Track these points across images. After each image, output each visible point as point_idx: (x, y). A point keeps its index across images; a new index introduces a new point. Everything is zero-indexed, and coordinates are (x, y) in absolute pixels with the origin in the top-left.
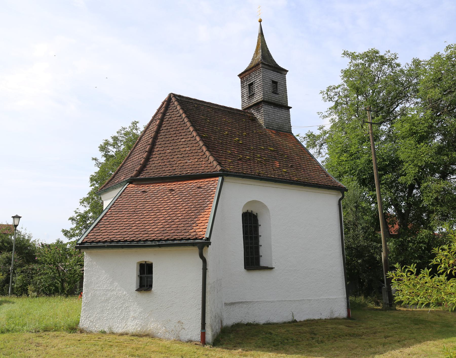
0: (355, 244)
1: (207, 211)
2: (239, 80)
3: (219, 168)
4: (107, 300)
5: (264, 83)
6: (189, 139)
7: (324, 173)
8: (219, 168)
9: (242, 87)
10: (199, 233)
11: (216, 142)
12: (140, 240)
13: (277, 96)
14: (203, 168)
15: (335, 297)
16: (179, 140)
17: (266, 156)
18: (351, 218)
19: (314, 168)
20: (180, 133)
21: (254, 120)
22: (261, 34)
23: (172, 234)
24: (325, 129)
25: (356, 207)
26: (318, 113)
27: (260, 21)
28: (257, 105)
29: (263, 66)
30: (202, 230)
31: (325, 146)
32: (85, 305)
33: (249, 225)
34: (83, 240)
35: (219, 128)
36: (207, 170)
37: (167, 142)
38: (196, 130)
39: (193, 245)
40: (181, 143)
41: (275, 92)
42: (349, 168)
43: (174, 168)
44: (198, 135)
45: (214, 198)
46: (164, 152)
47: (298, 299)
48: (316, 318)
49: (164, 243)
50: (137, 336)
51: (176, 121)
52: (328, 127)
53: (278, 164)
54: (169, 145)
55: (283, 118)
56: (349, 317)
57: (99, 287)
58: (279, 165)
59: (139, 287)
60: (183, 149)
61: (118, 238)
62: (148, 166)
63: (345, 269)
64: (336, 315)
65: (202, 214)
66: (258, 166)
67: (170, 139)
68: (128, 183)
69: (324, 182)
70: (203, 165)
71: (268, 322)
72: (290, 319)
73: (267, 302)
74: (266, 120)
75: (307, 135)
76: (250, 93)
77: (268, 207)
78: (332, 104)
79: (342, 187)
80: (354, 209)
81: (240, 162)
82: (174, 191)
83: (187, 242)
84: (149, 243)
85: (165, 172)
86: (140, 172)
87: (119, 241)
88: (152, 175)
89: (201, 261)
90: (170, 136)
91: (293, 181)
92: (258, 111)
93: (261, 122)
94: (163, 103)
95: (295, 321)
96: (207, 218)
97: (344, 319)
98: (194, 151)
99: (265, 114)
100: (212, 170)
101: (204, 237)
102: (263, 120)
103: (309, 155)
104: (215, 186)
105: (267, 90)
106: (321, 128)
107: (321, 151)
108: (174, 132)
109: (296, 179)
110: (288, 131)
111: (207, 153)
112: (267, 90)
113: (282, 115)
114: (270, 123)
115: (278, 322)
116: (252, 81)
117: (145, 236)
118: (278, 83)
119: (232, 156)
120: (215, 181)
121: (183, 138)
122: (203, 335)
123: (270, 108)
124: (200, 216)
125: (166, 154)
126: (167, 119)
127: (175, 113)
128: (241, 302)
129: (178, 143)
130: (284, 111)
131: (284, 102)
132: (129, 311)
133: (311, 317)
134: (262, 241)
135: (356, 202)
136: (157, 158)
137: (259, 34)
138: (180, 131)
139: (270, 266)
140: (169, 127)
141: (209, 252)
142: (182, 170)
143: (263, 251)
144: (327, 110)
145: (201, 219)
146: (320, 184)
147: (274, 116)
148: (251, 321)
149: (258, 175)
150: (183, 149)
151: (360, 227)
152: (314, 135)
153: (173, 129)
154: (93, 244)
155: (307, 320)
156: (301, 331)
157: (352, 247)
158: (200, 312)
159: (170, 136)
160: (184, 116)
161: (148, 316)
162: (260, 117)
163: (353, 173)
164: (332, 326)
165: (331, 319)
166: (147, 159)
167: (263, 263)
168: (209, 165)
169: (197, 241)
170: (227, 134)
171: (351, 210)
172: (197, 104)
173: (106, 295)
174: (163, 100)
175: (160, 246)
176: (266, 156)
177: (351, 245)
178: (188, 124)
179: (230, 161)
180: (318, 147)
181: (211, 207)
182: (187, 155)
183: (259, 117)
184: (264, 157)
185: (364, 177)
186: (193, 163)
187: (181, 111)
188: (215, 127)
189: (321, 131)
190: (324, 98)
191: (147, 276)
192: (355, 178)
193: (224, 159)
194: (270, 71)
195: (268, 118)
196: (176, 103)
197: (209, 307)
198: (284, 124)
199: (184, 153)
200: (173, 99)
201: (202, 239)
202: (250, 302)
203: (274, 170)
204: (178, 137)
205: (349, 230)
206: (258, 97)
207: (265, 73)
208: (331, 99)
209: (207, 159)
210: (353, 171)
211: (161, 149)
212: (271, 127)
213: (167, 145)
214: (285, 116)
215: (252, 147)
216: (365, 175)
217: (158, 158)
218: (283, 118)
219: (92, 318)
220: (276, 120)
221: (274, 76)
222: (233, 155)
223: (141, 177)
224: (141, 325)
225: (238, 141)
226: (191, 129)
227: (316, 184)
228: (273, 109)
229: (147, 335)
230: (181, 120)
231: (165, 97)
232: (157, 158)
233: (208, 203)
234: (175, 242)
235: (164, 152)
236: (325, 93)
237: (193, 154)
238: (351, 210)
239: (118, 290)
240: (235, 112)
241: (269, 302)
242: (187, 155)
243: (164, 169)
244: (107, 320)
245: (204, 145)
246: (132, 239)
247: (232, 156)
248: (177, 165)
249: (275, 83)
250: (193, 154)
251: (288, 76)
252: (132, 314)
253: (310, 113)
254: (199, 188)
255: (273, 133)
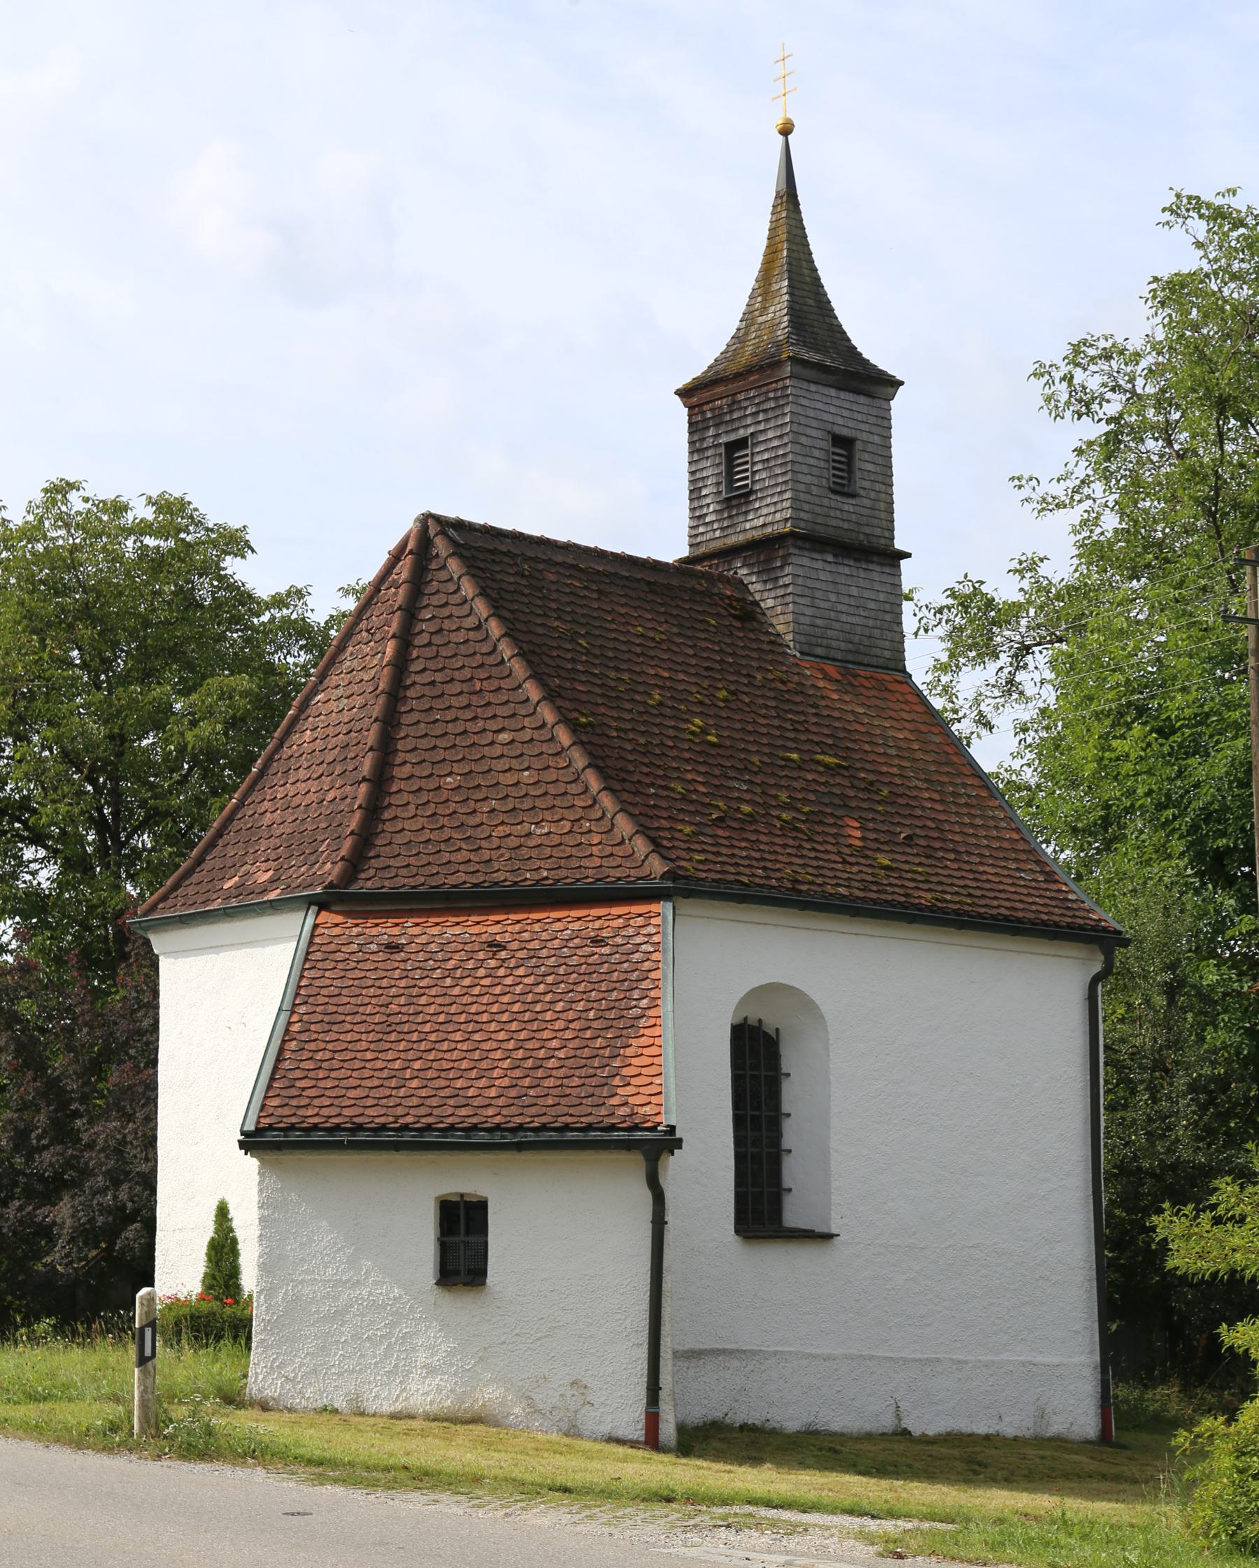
0: (1155, 1154)
1: (647, 1032)
2: (680, 413)
3: (657, 866)
4: (339, 1315)
5: (798, 448)
6: (527, 735)
7: (1038, 862)
8: (657, 866)
9: (697, 449)
10: (642, 1110)
11: (628, 746)
12: (452, 1127)
13: (848, 505)
14: (597, 862)
15: (1056, 1360)
16: (489, 737)
17: (812, 797)
18: (1144, 1037)
19: (996, 844)
20: (489, 704)
21: (749, 614)
22: (788, 197)
23: (552, 1111)
24: (1044, 570)
25: (1171, 991)
26: (1018, 481)
27: (786, 131)
28: (764, 550)
29: (800, 370)
30: (647, 1099)
31: (1039, 659)
32: (265, 1329)
33: (749, 1073)
34: (258, 1122)
35: (625, 677)
36: (613, 873)
37: (439, 742)
38: (551, 696)
39: (627, 1145)
40: (497, 750)
41: (843, 487)
42: (1149, 793)
43: (486, 855)
44: (565, 720)
45: (661, 984)
46: (432, 784)
47: (918, 1356)
48: (982, 1429)
49: (531, 1137)
50: (446, 1420)
51: (463, 649)
52: (1062, 567)
53: (858, 834)
54: (449, 755)
55: (872, 605)
56: (1104, 1437)
57: (307, 1272)
58: (863, 839)
59: (438, 1276)
60: (510, 778)
61: (374, 1115)
62: (379, 842)
63: (1103, 1269)
64: (1057, 1427)
65: (634, 1042)
66: (785, 846)
67: (451, 728)
68: (314, 909)
69: (1035, 907)
70: (595, 850)
71: (813, 1428)
72: (886, 1423)
73: (809, 1356)
74: (803, 620)
75: (953, 594)
76: (730, 488)
77: (824, 1009)
78: (1094, 430)
79: (1105, 929)
80: (1160, 1001)
81: (720, 832)
82: (505, 948)
83: (606, 1136)
84: (482, 1137)
85: (453, 868)
86: (355, 863)
87: (383, 1127)
88: (405, 882)
89: (646, 1196)
90: (450, 715)
91: (919, 907)
92: (768, 573)
93: (781, 629)
94: (396, 557)
95: (906, 1433)
96: (656, 1060)
97: (1088, 1442)
98: (552, 789)
99: (799, 591)
100: (633, 872)
101: (659, 1124)
102: (790, 618)
103: (976, 782)
104: (656, 939)
105: (808, 479)
106: (1027, 566)
107: (1019, 677)
108: (463, 700)
109: (926, 898)
110: (892, 664)
111: (607, 801)
112: (808, 479)
113: (867, 594)
114: (818, 632)
115: (845, 1430)
116: (742, 433)
117: (463, 1112)
118: (859, 445)
119: (692, 808)
120: (648, 916)
121: (502, 730)
122: (652, 1421)
123: (820, 565)
124: (629, 1052)
125: (445, 795)
126: (425, 638)
127: (456, 611)
128: (724, 1352)
129: (487, 751)
130: (876, 572)
131: (878, 532)
132: (414, 1350)
133: (964, 1425)
134: (790, 1137)
135: (1172, 967)
136: (411, 810)
137: (778, 196)
138: (489, 697)
139: (820, 1228)
140: (439, 677)
141: (674, 1168)
142: (517, 865)
143: (793, 1172)
144: (1062, 471)
145: (635, 1061)
146: (1019, 920)
147: (833, 598)
148: (755, 1418)
149: (793, 889)
150: (510, 778)
151: (1181, 1081)
152: (990, 603)
153: (457, 687)
154: (294, 1136)
155: (949, 1434)
156: (934, 1453)
157: (1139, 1169)
158: (643, 1353)
159: (450, 715)
160: (495, 628)
161: (474, 1366)
162: (779, 605)
163: (1167, 822)
164: (1042, 1453)
165: (1040, 1441)
166: (374, 810)
167: (793, 1216)
168: (618, 851)
169: (639, 1135)
170: (661, 704)
171: (1147, 1001)
172: (528, 559)
173: (336, 1299)
174: (393, 543)
175: (520, 1147)
176: (812, 797)
177: (1135, 1158)
178: (518, 668)
179: (688, 830)
180: (1004, 659)
181: (658, 1021)
182: (527, 804)
183: (770, 603)
184: (805, 801)
185: (1222, 842)
186: (556, 840)
187: (481, 608)
188: (613, 674)
189: (1026, 584)
190: (1048, 399)
191: (466, 1239)
192: (1177, 845)
193: (665, 824)
194: (826, 391)
195: (808, 611)
196: (454, 566)
197: (669, 1339)
198: (876, 633)
199: (513, 792)
200: (441, 546)
201: (653, 1129)
202: (754, 1353)
203: (844, 862)
204: (480, 724)
205: (1133, 1092)
206: (769, 514)
207: (796, 390)
208: (1085, 404)
209: (605, 825)
210: (1169, 813)
211: (418, 771)
212: (819, 651)
213: (441, 755)
214: (882, 597)
215: (755, 759)
216: (1223, 834)
217: (412, 807)
218: (872, 605)
219: (290, 1368)
220: (844, 618)
221: (838, 410)
222: (692, 802)
223: (365, 884)
224: (452, 1391)
225: (704, 731)
226: (532, 691)
227: (1006, 918)
228: (833, 568)
229: (475, 1420)
230: (486, 648)
231: (398, 526)
232: (411, 810)
233: (644, 1003)
234: (570, 1135)
235: (432, 784)
236: (1057, 376)
237: (549, 801)
238: (1147, 1001)
239: (375, 1283)
240: (675, 582)
241: (815, 1357)
242: (527, 804)
243: (446, 857)
244: (339, 1375)
245: (589, 766)
246: (424, 1120)
247: (692, 808)
248: (496, 842)
249: (843, 443)
250: (549, 801)
251: (899, 406)
252: (422, 1357)
253: (984, 502)
254: (597, 941)
255: (831, 680)
